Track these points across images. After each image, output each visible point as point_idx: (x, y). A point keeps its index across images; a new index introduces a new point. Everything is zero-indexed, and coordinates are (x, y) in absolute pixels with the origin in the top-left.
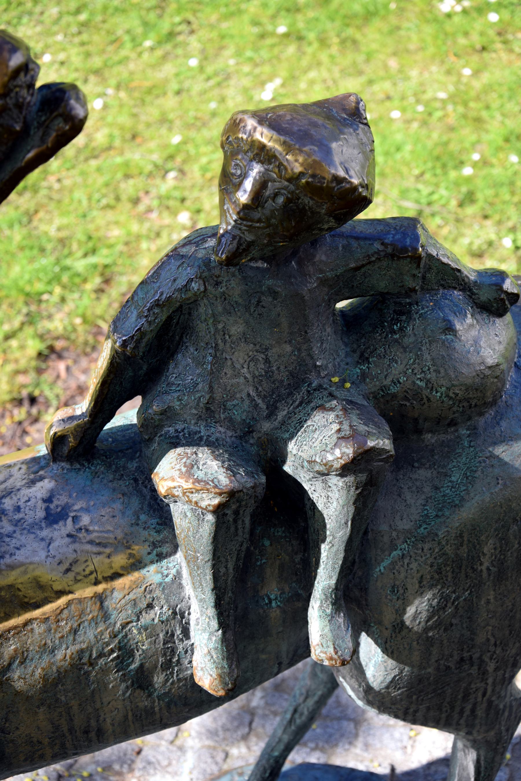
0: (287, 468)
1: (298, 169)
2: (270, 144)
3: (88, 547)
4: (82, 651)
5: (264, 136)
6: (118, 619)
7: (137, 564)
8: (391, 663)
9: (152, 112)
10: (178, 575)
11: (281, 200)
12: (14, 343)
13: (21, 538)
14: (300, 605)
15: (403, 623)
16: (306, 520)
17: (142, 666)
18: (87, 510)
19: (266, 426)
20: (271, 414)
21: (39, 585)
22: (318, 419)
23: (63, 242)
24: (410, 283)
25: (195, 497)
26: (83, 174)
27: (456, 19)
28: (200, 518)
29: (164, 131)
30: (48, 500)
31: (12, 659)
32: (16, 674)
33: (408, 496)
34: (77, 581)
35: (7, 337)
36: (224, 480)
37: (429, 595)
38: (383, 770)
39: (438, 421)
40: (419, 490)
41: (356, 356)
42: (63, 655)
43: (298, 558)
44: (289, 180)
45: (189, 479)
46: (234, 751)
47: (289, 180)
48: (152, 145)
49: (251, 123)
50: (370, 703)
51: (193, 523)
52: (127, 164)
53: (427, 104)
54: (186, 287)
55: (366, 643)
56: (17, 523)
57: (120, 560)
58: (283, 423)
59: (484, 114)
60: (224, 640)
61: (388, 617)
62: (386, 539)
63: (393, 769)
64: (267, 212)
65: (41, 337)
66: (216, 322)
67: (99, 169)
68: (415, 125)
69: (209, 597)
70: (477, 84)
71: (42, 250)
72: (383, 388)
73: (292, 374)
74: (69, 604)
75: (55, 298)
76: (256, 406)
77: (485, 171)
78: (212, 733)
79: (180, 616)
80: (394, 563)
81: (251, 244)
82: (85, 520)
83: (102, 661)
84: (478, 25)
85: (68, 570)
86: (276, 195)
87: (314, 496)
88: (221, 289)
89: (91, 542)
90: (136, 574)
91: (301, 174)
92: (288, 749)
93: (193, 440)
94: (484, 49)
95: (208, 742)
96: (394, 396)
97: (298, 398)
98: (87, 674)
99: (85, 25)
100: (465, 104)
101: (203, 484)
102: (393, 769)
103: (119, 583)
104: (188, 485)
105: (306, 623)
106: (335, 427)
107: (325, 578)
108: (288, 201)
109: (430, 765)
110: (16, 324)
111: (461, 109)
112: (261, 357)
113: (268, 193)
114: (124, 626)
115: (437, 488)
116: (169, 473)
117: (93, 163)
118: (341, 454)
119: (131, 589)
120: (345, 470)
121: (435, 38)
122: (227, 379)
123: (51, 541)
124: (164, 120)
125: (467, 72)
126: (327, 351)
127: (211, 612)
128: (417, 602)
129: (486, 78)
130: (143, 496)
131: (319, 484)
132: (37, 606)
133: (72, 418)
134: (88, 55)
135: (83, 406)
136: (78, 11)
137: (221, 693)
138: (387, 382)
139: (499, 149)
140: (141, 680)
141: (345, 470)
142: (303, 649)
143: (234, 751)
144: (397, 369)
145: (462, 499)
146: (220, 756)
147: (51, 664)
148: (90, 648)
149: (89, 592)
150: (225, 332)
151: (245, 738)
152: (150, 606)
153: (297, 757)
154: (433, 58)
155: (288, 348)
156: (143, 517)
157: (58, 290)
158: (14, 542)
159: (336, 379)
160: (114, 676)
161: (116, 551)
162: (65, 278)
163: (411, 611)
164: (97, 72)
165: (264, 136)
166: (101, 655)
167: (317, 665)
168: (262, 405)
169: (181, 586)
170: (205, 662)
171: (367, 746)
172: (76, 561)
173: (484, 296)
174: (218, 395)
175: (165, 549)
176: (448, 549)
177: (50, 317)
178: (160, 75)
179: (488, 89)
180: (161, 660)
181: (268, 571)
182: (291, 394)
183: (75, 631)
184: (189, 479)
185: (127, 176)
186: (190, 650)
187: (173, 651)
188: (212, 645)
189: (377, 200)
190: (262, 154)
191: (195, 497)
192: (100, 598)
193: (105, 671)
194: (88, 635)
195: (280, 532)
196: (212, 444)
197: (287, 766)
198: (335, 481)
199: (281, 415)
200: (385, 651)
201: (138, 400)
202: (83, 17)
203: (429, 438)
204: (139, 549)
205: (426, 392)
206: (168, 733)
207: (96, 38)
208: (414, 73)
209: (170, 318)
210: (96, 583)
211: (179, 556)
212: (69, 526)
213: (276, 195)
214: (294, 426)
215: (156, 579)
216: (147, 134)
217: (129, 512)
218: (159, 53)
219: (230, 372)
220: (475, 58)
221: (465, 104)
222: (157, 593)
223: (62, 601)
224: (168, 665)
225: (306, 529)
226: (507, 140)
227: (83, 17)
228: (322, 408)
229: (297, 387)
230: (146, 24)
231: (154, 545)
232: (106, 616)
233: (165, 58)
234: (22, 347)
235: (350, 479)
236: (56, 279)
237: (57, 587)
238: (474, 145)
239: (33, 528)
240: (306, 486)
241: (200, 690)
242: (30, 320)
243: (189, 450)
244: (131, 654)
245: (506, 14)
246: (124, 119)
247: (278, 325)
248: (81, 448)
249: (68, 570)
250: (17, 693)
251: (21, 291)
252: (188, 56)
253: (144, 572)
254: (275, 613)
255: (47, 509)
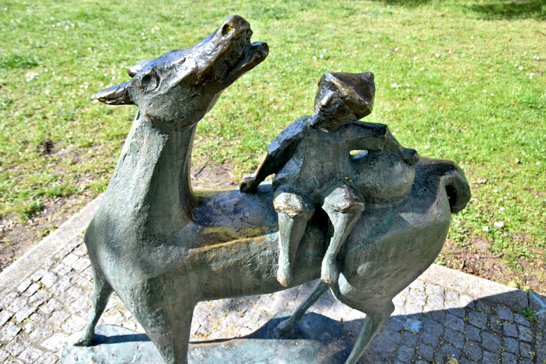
0: (324, 207)
1: (345, 94)
2: (336, 84)
3: (247, 224)
4: (238, 261)
5: (335, 81)
6: (253, 252)
7: (263, 233)
8: (349, 286)
9: (298, 103)
10: (277, 240)
11: (337, 106)
12: (245, 163)
13: (223, 217)
14: (331, 325)
15: (356, 272)
16: (327, 228)
17: (259, 270)
18: (249, 211)
19: (318, 191)
20: (320, 187)
21: (227, 234)
22: (338, 190)
23: (265, 136)
24: (380, 147)
25: (287, 211)
26: (275, 117)
27: (396, 90)
28: (288, 220)
29: (302, 109)
30: (236, 205)
31: (213, 259)
32: (213, 265)
33: (366, 225)
34: (240, 235)
35: (243, 161)
36: (299, 207)
37: (368, 264)
38: (339, 319)
39: (382, 200)
40: (371, 224)
41: (355, 171)
42: (231, 261)
43: (322, 241)
44: (342, 98)
45: (286, 204)
46: (290, 303)
47: (342, 98)
48: (298, 112)
49: (330, 76)
50: (338, 298)
51: (284, 221)
52: (289, 117)
53: (384, 112)
54: (297, 135)
55: (341, 275)
56: (223, 211)
57: (257, 231)
58: (324, 191)
59: (402, 118)
60: (290, 266)
61: (352, 269)
62: (355, 240)
63: (342, 320)
64: (331, 109)
65: (254, 163)
66: (306, 149)
67: (280, 117)
68: (379, 118)
69: (287, 249)
70: (400, 109)
71: (259, 137)
72: (364, 184)
73: (331, 173)
74: (236, 243)
75: (260, 152)
76: (316, 183)
77: (400, 134)
78: (284, 296)
79: (275, 255)
80: (357, 250)
81: (323, 121)
82: (247, 214)
83: (245, 266)
84: (403, 92)
85: (238, 231)
86: (336, 103)
87: (331, 219)
88: (310, 138)
89: (248, 222)
90: (262, 237)
91: (347, 96)
92: (308, 307)
93: (291, 191)
94: (404, 99)
95: (282, 299)
96: (367, 188)
97: (332, 182)
98: (239, 269)
99: (284, 76)
100: (396, 114)
101: (291, 207)
102: (342, 320)
103: (256, 239)
104: (286, 206)
105: (321, 265)
106: (344, 194)
107: (331, 251)
108: (340, 106)
109: (355, 321)
110: (247, 158)
111: (394, 115)
112: (320, 165)
113: (333, 102)
114: (255, 254)
115: (377, 225)
116: (280, 201)
117: (279, 115)
118: (344, 204)
119: (259, 242)
120: (345, 211)
121: (389, 94)
122: (307, 170)
123: (234, 219)
124: (302, 106)
125: (398, 105)
126: (344, 168)
127: (287, 255)
128: (363, 265)
129: (403, 108)
130: (270, 210)
131: (334, 215)
132: (225, 242)
133: (250, 178)
134: (283, 85)
135: (254, 175)
136: (283, 72)
137: (286, 285)
138: (366, 182)
139: (405, 129)
140: (258, 275)
141: (345, 211)
142: (318, 275)
143: (290, 303)
144: (369, 178)
145: (386, 231)
146: (285, 304)
147: (226, 264)
148: (241, 260)
149: (244, 240)
150: (308, 153)
151: (294, 300)
152: (265, 249)
153: (311, 309)
154: (387, 100)
155: (331, 164)
156: (268, 217)
157: (261, 150)
158: (221, 218)
159: (346, 178)
160: (248, 272)
161: (257, 227)
162: (264, 146)
163: (360, 268)
164: (285, 90)
165: (335, 81)
166: (245, 264)
167: (322, 282)
168: (318, 183)
169: (277, 244)
170: (281, 274)
171: (334, 310)
172: (241, 228)
173: (406, 157)
174: (302, 176)
175: (274, 229)
176: (378, 248)
177: (257, 157)
178: (303, 93)
179: (403, 111)
180: (266, 269)
181: (310, 244)
182: (329, 181)
183: (237, 253)
184: (286, 204)
185: (288, 120)
186: (277, 268)
187: (271, 267)
188: (285, 267)
189: (373, 113)
190: (333, 87)
191: (287, 211)
192: (248, 243)
193: (246, 270)
194: (241, 255)
195: (317, 231)
196: (298, 194)
197: (306, 312)
198: (341, 215)
199: (324, 188)
200: (348, 281)
201: (274, 174)
202: (284, 74)
203: (377, 206)
204: (265, 228)
205: (379, 188)
206: (270, 294)
207: (287, 81)
208: (381, 103)
209: (289, 146)
210: (247, 237)
211: (279, 233)
212: (241, 215)
213: (336, 103)
214: (328, 192)
215: (269, 240)
216: (297, 109)
217: (264, 214)
218: (304, 87)
219: (308, 168)
220: (401, 102)
221: (396, 114)
222: (269, 245)
223: (234, 241)
224: (268, 272)
225: (327, 231)
226: (408, 126)
227: (284, 74)
228: (340, 187)
229: (332, 178)
230: (302, 78)
231: (270, 227)
232: (249, 250)
233: (306, 88)
234: (247, 165)
235: (346, 215)
236: (261, 146)
237: (233, 236)
238: (397, 126)
239: (228, 214)
240: (329, 215)
241: (279, 283)
242: (251, 157)
243: (288, 194)
244: (256, 266)
245: (412, 91)
246: (291, 104)
247: (329, 154)
248: (251, 188)
249: (238, 231)
250: (213, 272)
251: (250, 148)
252: (313, 89)
253: (265, 236)
254: (310, 260)
255: (235, 208)
